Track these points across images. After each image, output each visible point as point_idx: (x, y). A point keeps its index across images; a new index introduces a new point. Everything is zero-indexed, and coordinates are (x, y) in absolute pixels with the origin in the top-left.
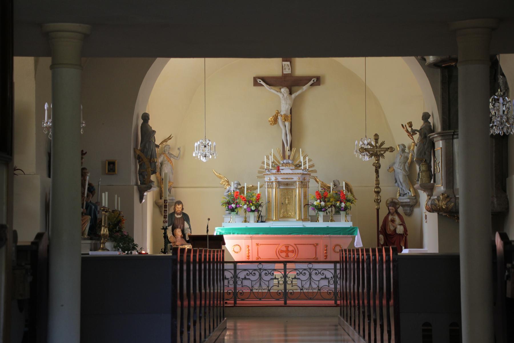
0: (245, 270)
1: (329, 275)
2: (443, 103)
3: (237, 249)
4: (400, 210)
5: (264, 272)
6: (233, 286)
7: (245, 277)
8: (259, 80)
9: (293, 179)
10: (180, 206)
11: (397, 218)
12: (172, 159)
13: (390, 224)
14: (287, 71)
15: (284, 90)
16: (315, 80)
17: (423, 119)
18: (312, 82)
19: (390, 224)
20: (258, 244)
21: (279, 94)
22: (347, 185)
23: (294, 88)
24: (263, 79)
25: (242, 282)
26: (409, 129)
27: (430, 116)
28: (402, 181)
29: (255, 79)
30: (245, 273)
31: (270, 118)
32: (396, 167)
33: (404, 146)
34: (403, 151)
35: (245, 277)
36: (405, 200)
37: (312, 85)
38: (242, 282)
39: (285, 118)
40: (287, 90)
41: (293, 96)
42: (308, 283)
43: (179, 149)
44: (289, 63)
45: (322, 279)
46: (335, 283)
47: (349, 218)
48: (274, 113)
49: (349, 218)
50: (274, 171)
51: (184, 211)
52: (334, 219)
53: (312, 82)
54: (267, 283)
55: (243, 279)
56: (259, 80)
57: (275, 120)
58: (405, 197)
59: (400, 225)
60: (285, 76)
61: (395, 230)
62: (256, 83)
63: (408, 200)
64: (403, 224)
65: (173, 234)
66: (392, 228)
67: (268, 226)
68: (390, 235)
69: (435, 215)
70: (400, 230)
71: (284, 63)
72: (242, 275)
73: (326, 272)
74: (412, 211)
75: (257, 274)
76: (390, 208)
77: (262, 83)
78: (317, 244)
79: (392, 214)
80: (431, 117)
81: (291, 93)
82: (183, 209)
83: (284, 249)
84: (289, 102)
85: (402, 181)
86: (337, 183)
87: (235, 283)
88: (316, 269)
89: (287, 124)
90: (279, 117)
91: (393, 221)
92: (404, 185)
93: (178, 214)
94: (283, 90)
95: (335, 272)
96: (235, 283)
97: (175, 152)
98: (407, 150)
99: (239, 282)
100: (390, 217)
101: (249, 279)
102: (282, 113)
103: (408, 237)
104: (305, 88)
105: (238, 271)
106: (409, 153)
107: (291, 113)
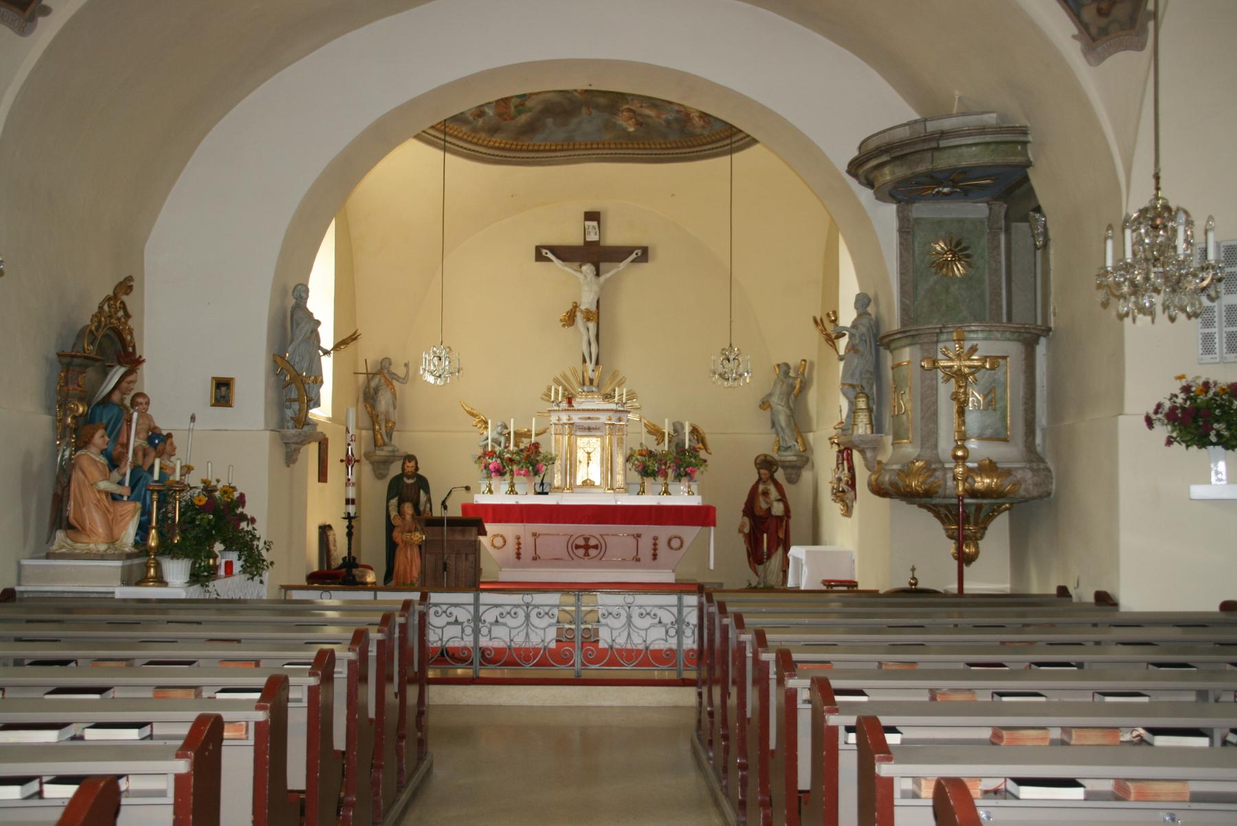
0: (497, 606)
1: (668, 618)
2: (901, 274)
3: (499, 542)
4: (780, 475)
5: (536, 611)
6: (471, 638)
7: (497, 621)
8: (544, 251)
9: (323, 477)
10: (413, 463)
11: (772, 489)
12: (395, 382)
13: (761, 499)
14: (592, 237)
15: (588, 269)
16: (639, 252)
17: (856, 308)
18: (633, 256)
19: (761, 499)
20: (534, 535)
21: (578, 274)
22: (694, 431)
23: (603, 266)
24: (553, 249)
25: (490, 631)
26: (830, 328)
27: (870, 301)
28: (783, 424)
29: (538, 249)
30: (496, 612)
31: (563, 314)
32: (775, 400)
33: (787, 365)
34: (786, 374)
35: (497, 621)
36: (789, 457)
37: (633, 261)
38: (490, 631)
39: (588, 316)
40: (593, 268)
41: (602, 279)
42: (626, 633)
43: (406, 365)
44: (595, 223)
45: (448, 624)
46: (680, 633)
47: (694, 487)
48: (570, 307)
49: (694, 487)
50: (564, 405)
51: (420, 472)
52: (670, 488)
53: (633, 256)
54: (541, 633)
55: (492, 624)
56: (544, 251)
57: (570, 319)
58: (788, 453)
59: (778, 500)
60: (588, 244)
61: (769, 510)
62: (540, 257)
63: (795, 458)
64: (783, 499)
65: (399, 511)
66: (764, 506)
67: (554, 503)
68: (761, 517)
69: (165, 433)
70: (778, 509)
71: (587, 223)
72: (489, 616)
73: (661, 613)
74: (799, 476)
75: (521, 613)
76: (762, 471)
77: (550, 255)
78: (639, 536)
79: (764, 482)
80: (872, 304)
81: (598, 274)
82: (417, 469)
83: (581, 542)
84: (595, 288)
85: (783, 424)
86: (679, 427)
87: (476, 632)
88: (640, 607)
89: (592, 325)
90: (578, 314)
91: (766, 493)
92: (787, 431)
93: (409, 478)
94: (584, 268)
95: (680, 633)
96: (476, 632)
97: (401, 372)
98: (792, 374)
99: (484, 631)
100: (761, 487)
101: (505, 624)
102: (583, 307)
103: (792, 522)
104: (622, 265)
105: (482, 609)
106: (795, 378)
107: (598, 307)
